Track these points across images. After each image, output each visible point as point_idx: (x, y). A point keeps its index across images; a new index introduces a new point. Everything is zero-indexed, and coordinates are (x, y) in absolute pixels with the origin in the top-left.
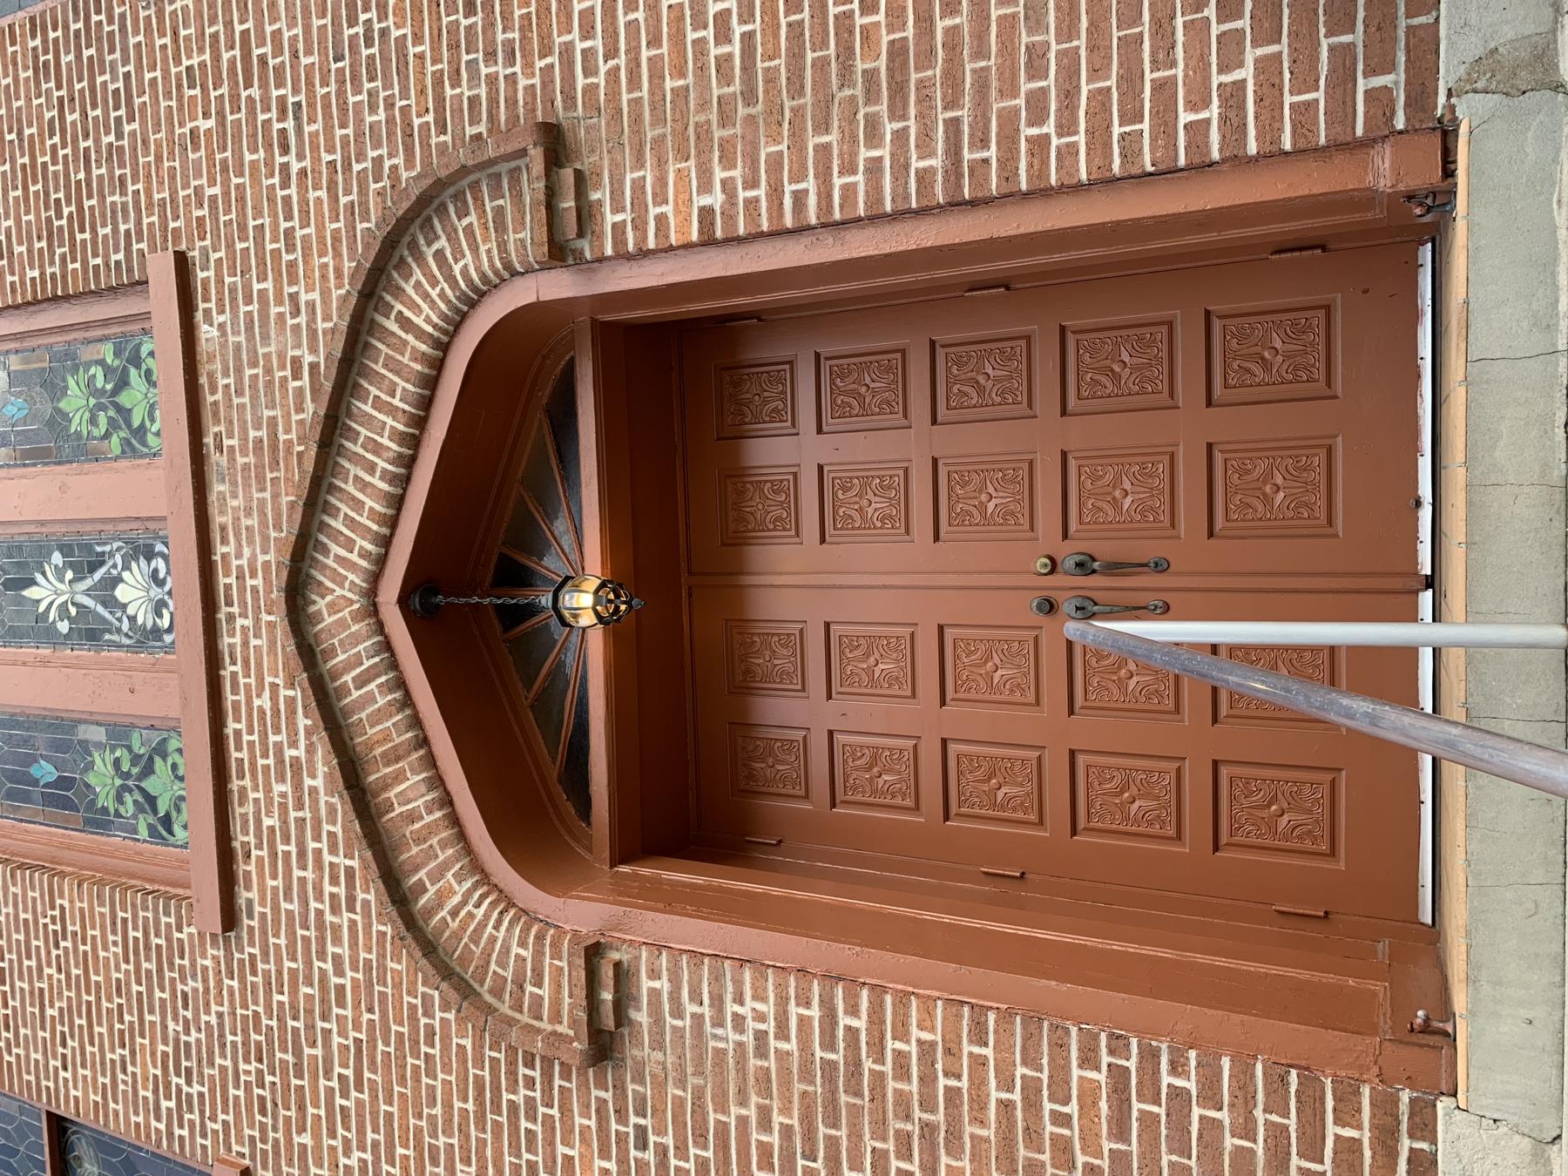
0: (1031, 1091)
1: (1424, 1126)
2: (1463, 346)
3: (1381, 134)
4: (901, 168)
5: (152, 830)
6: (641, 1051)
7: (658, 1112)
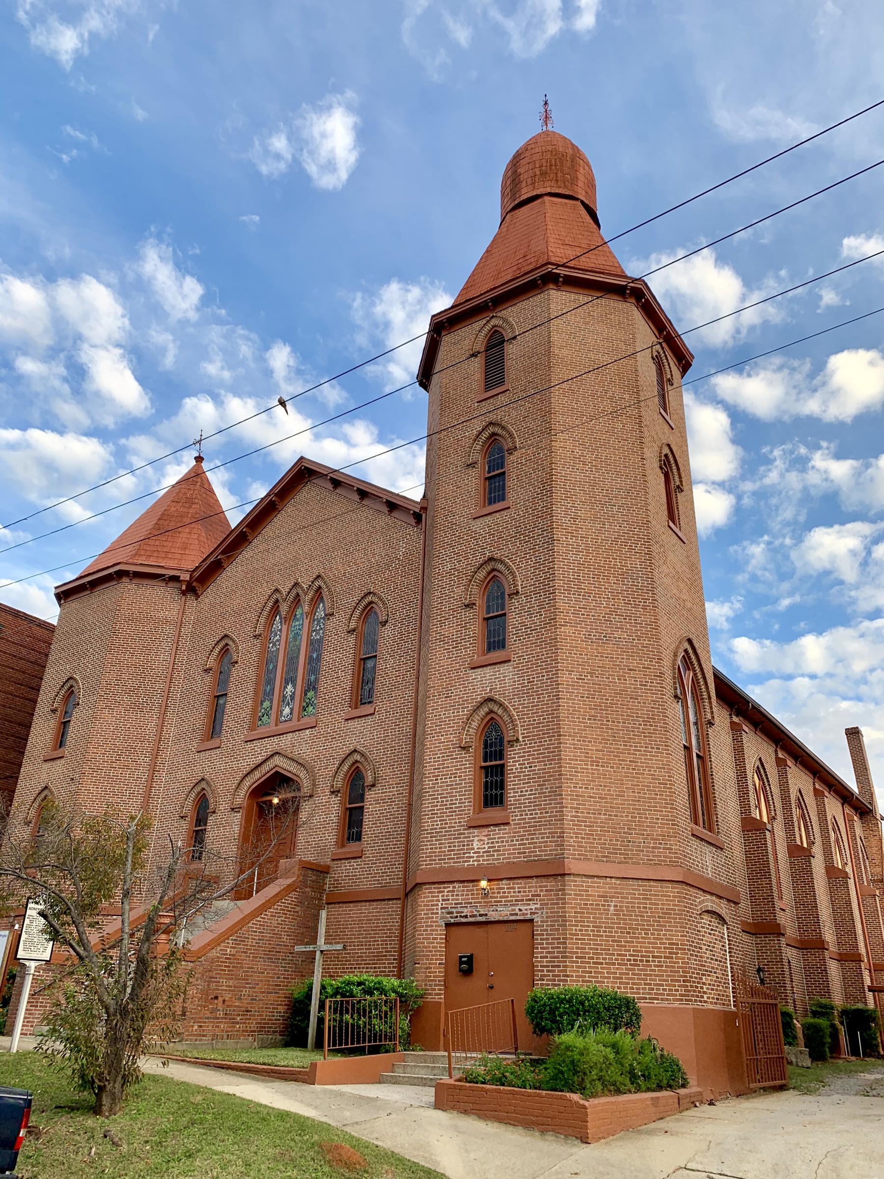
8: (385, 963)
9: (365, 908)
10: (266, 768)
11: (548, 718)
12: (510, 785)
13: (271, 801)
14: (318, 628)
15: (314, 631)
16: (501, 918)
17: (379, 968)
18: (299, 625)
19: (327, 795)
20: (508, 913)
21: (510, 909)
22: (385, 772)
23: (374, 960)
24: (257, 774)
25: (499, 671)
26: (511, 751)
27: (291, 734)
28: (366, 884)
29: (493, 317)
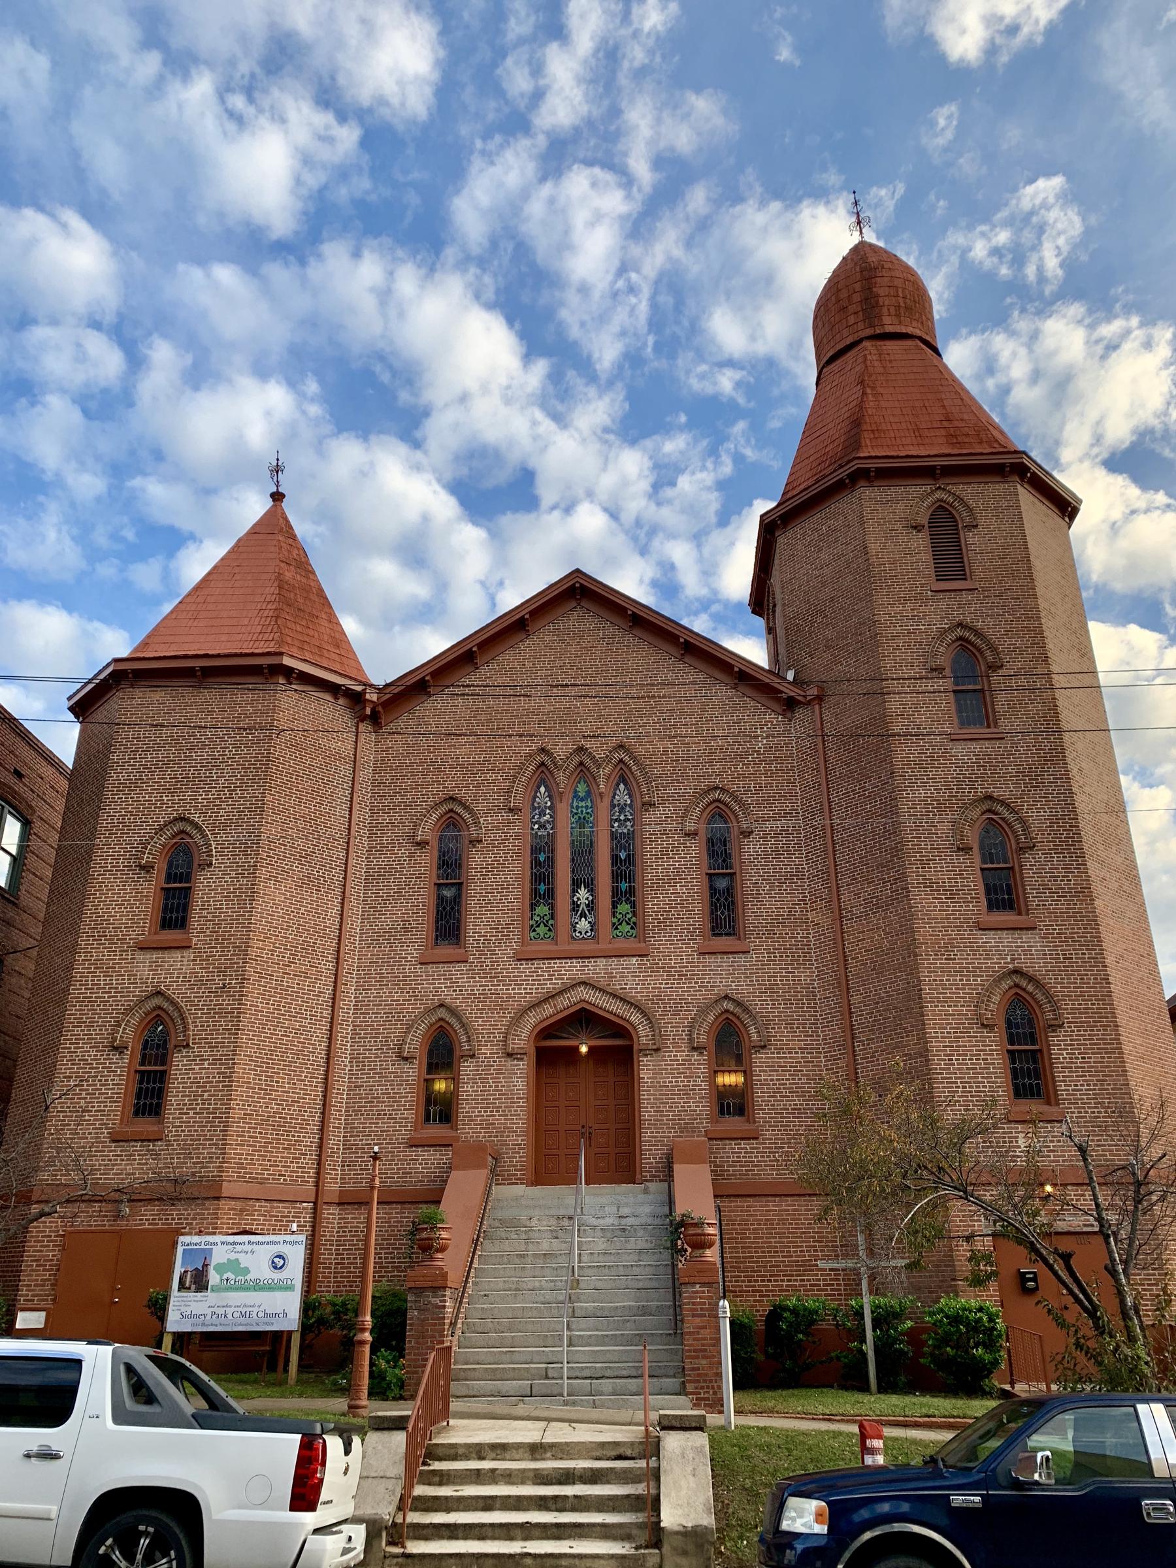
0: (516, 1132)
1: (521, 1184)
2: (625, 1373)
3: (642, 1176)
4: (646, 1112)
5: (532, 926)
6: (510, 1063)
7: (500, 1065)
8: (817, 1275)
9: (773, 1204)
10: (563, 1002)
11: (1099, 1004)
12: (1059, 1077)
13: (577, 1048)
14: (622, 817)
15: (616, 820)
16: (1072, 1229)
17: (809, 1280)
18: (587, 807)
19: (684, 1051)
20: (1081, 1223)
21: (1082, 1219)
22: (778, 1030)
23: (800, 1271)
24: (548, 1010)
25: (1021, 938)
26: (1053, 1037)
27: (602, 959)
28: (768, 1174)
29: (939, 488)
